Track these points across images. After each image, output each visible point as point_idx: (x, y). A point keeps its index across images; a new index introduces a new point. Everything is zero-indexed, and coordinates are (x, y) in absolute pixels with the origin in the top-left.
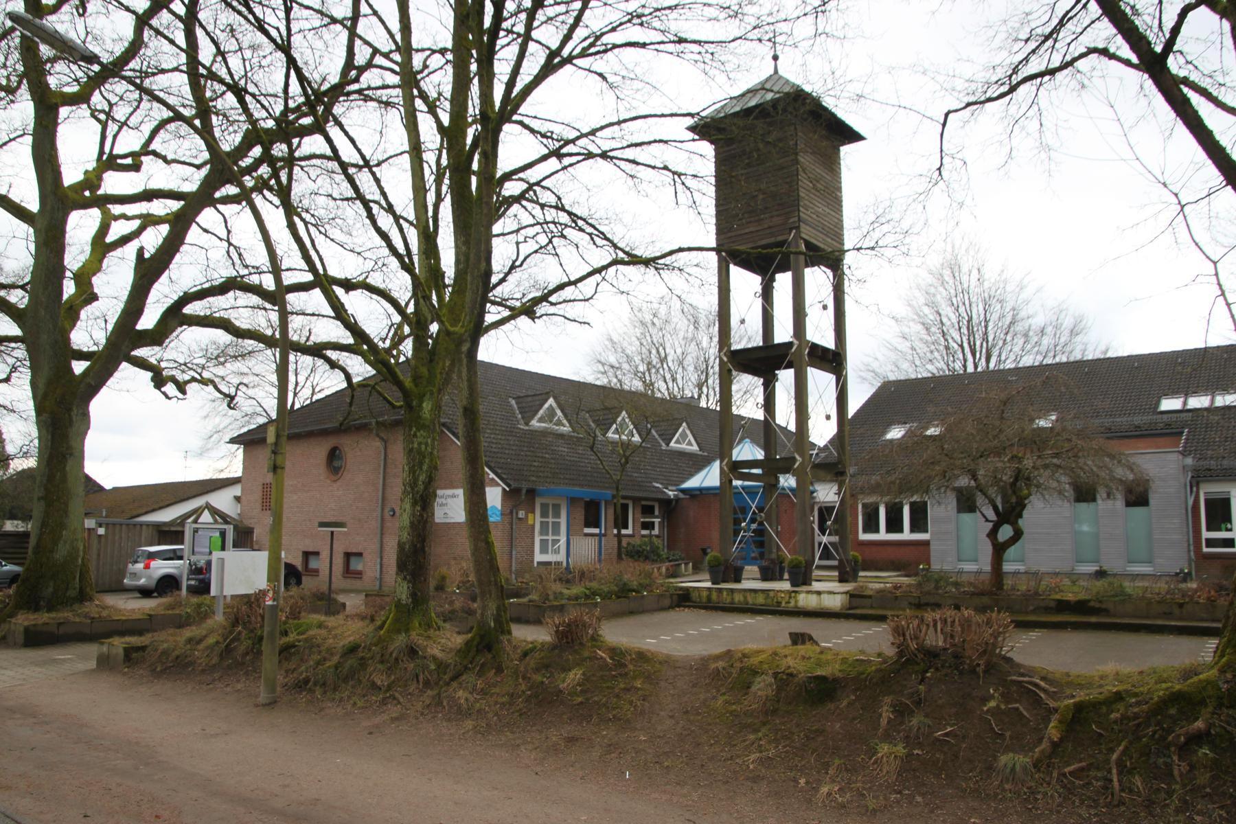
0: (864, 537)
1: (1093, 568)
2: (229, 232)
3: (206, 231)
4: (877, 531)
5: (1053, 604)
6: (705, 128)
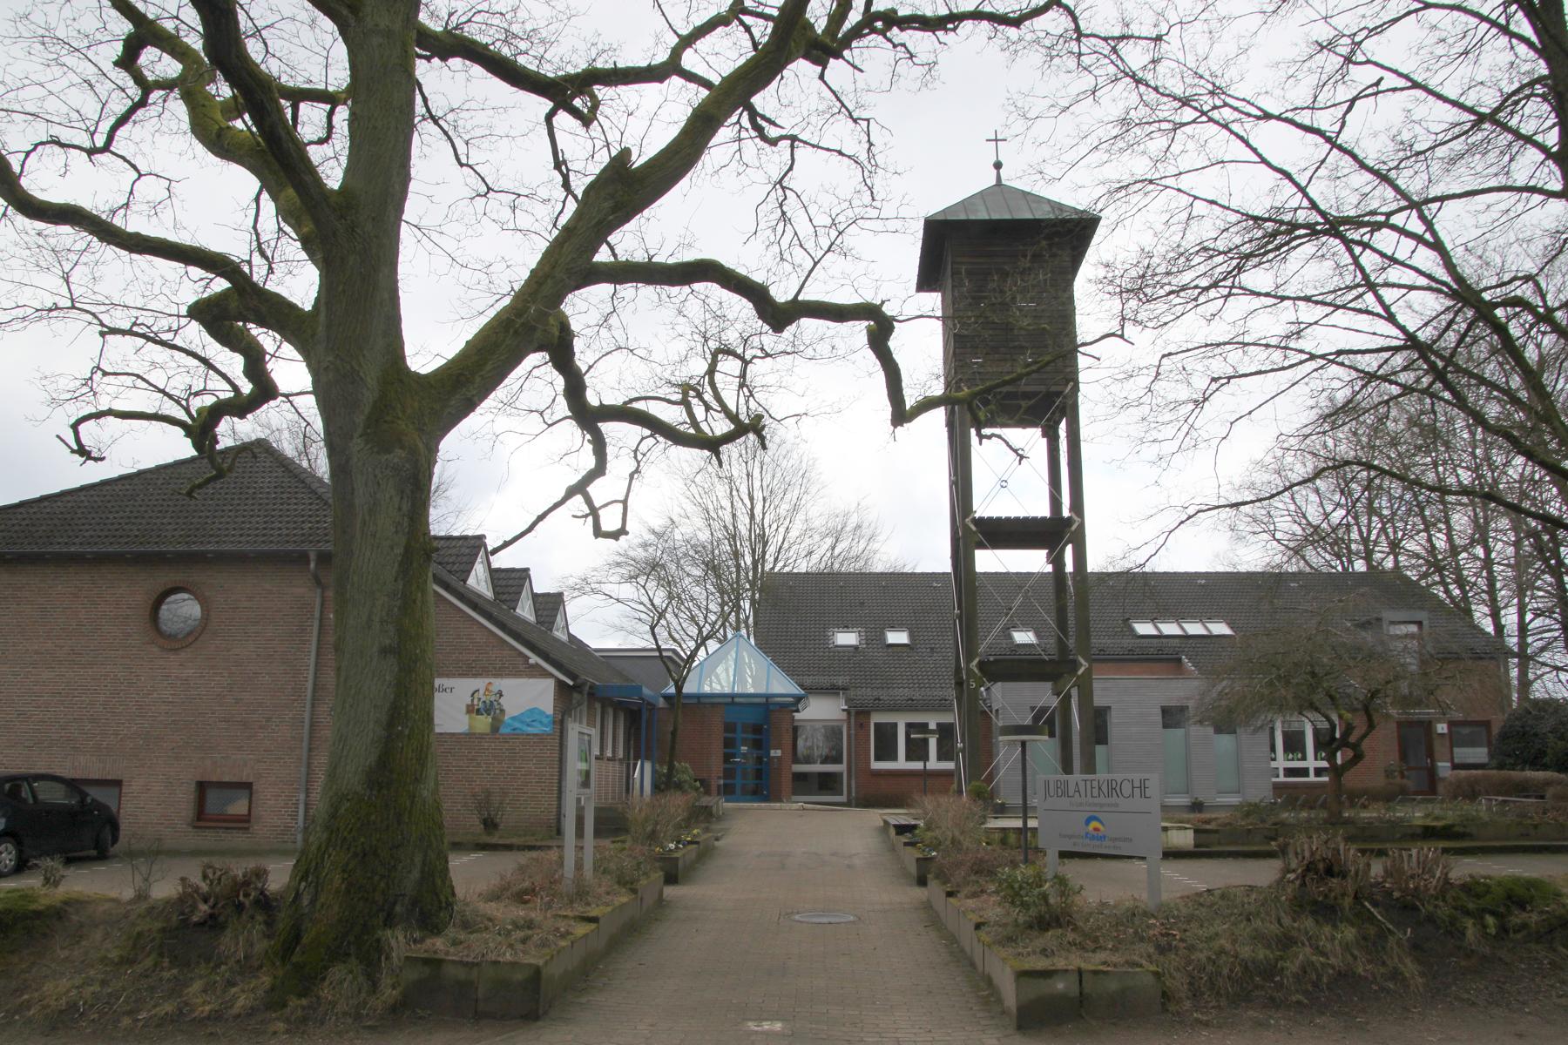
1: (1184, 800)
3: (1212, 202)
4: (894, 758)
5: (1419, 831)
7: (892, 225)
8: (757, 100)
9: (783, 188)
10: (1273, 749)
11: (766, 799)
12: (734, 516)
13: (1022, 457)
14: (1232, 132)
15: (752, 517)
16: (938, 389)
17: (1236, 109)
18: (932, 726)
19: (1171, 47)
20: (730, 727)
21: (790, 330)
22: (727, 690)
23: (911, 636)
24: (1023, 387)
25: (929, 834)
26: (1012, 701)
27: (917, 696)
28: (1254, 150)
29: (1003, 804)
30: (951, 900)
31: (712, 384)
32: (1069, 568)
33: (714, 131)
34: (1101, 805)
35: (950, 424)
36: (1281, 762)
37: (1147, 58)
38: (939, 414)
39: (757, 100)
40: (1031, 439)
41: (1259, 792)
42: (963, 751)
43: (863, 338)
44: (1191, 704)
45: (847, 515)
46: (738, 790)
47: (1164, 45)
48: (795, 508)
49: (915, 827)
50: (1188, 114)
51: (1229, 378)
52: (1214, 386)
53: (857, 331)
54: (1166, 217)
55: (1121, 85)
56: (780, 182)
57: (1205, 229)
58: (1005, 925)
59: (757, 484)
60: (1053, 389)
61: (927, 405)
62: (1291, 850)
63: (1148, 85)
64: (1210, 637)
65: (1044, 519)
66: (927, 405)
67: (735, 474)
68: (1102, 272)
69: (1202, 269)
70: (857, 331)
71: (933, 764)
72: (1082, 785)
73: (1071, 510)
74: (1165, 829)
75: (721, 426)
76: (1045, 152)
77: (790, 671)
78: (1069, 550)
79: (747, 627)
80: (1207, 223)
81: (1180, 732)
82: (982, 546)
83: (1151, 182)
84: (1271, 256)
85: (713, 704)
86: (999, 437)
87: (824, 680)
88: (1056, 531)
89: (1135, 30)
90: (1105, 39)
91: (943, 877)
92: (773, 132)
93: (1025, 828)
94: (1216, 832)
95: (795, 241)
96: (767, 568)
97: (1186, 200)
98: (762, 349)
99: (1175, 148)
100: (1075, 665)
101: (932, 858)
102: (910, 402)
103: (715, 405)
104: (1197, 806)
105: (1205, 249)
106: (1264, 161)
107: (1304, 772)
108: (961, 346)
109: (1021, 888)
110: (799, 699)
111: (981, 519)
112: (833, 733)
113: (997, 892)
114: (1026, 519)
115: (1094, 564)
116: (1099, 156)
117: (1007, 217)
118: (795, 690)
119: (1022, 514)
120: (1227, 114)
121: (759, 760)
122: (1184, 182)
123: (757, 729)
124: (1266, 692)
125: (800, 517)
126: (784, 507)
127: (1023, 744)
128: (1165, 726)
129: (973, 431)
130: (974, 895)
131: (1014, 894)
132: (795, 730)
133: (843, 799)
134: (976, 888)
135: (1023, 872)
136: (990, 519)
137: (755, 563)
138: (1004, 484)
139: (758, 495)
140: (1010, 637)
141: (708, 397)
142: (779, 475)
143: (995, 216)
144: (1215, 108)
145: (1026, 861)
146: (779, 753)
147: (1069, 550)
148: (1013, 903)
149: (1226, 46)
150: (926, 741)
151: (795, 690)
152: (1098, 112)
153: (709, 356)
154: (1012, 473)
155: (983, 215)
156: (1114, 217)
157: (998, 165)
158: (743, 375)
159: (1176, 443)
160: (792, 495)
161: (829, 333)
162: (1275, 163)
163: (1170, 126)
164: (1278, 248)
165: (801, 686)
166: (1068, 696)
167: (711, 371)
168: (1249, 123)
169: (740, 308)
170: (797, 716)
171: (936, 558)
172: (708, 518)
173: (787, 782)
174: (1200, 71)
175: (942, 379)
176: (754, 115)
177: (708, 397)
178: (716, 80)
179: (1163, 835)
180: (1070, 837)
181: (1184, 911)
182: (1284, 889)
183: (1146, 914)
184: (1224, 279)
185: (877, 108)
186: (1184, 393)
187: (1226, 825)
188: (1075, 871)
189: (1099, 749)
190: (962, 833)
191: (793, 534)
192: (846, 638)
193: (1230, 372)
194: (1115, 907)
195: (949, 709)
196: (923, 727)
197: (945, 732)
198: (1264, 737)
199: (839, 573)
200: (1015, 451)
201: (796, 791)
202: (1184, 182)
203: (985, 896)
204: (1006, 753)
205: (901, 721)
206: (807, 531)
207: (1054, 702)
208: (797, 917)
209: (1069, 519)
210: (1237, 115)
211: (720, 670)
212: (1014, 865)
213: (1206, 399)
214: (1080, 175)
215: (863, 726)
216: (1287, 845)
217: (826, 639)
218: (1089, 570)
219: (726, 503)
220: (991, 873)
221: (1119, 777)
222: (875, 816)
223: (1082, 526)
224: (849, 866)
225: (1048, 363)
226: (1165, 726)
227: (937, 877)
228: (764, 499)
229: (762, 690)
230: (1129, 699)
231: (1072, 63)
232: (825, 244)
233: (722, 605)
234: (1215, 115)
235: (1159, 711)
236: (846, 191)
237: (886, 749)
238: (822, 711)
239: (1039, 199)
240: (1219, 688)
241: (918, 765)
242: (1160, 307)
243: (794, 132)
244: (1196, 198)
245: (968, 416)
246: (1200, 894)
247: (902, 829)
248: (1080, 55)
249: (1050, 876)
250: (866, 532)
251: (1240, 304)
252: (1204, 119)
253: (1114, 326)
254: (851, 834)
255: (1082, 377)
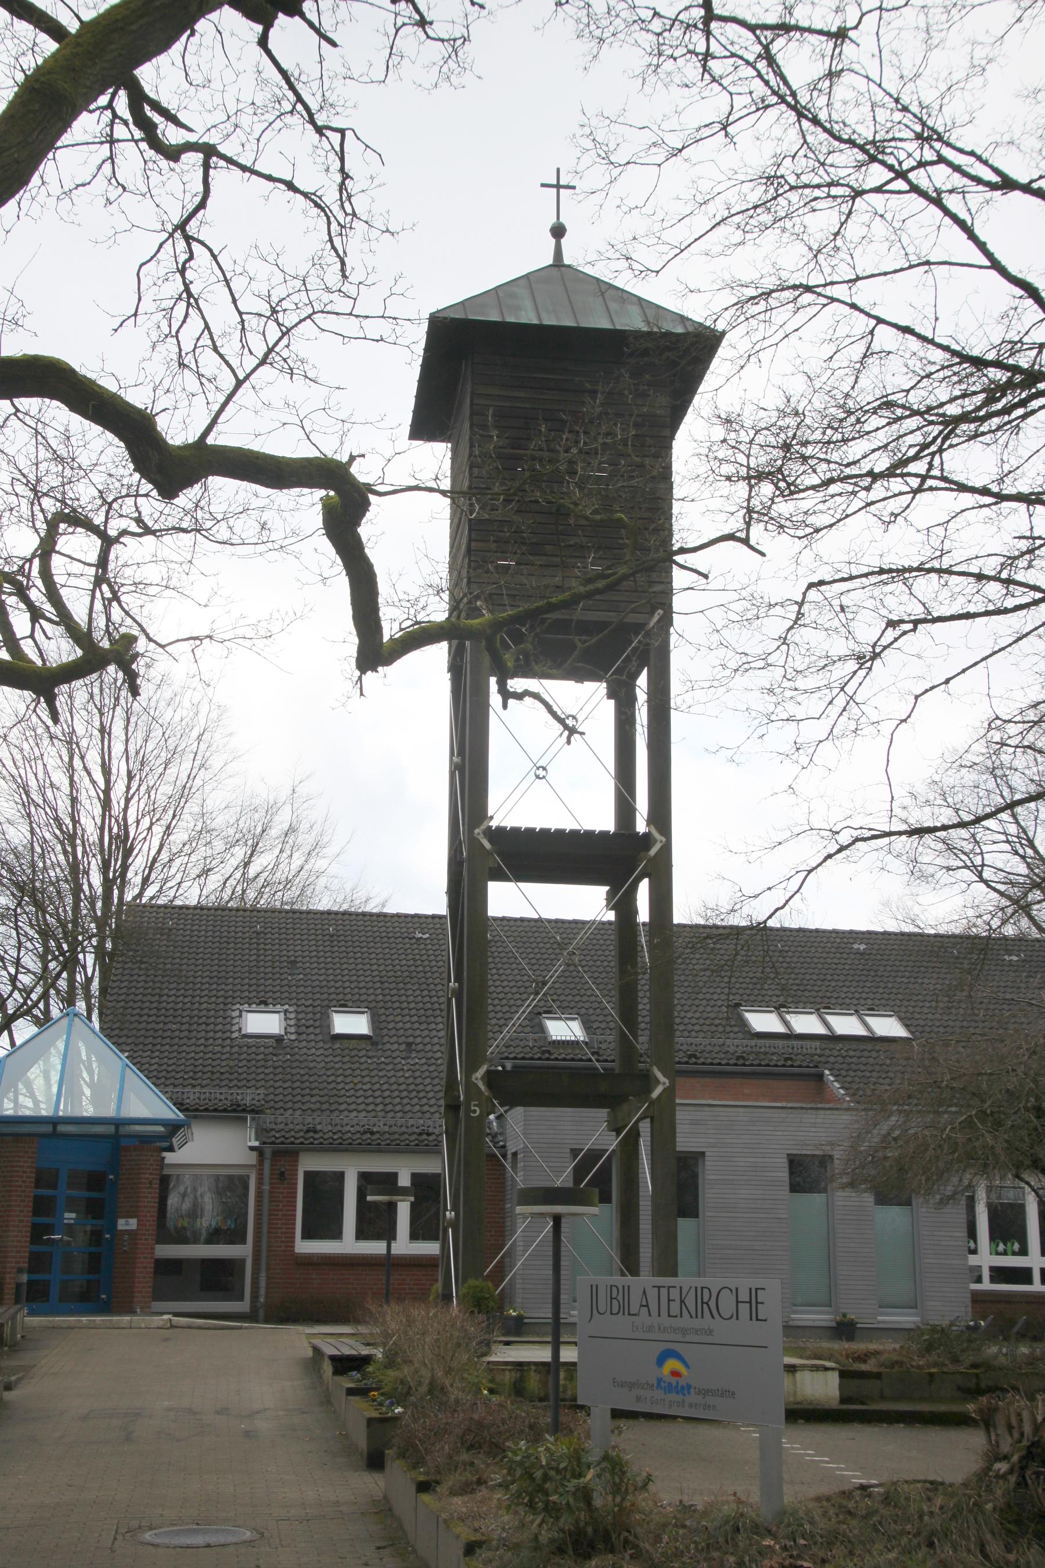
0: (305, 1247)
1: (822, 1318)
2: (104, 162)
3: (907, 330)
4: (336, 1234)
6: (723, 333)
7: (374, 329)
8: (146, 74)
9: (188, 239)
10: (972, 1234)
11: (106, 1308)
12: (74, 801)
13: (572, 731)
14: (947, 212)
15: (106, 804)
16: (438, 611)
17: (957, 169)
18: (404, 1181)
19: (857, 53)
20: (45, 1178)
21: (186, 498)
22: (45, 1111)
23: (374, 1022)
24: (579, 613)
25: (392, 1373)
26: (542, 1140)
27: (380, 1126)
28: (982, 246)
29: (520, 1319)
30: (426, 1498)
31: (46, 574)
32: (643, 915)
33: (65, 125)
34: (684, 1331)
35: (456, 669)
36: (986, 1258)
37: (820, 68)
38: (438, 653)
39: (146, 74)
40: (588, 700)
41: (948, 1308)
42: (454, 1224)
43: (315, 518)
44: (837, 1154)
45: (272, 810)
46: (55, 1291)
47: (848, 48)
48: (184, 794)
49: (367, 1360)
50: (877, 174)
51: (916, 623)
52: (891, 634)
53: (307, 505)
54: (829, 350)
55: (772, 113)
56: (182, 226)
57: (892, 376)
58: (517, 1547)
59: (118, 748)
60: (632, 618)
61: (419, 637)
62: (1000, 1420)
63: (815, 121)
64: (873, 1040)
65: (604, 834)
66: (419, 637)
67: (80, 728)
68: (719, 432)
69: (881, 438)
70: (307, 505)
71: (404, 1245)
72: (652, 1294)
73: (650, 822)
74: (791, 1369)
75: (60, 650)
76: (637, 224)
77: (159, 1078)
78: (644, 888)
79: (88, 997)
80: (894, 363)
81: (817, 1199)
82: (499, 876)
83: (808, 289)
84: (996, 421)
85: (18, 1137)
86: (536, 696)
87: (222, 1095)
88: (629, 855)
89: (801, 16)
90: (752, 28)
91: (413, 1454)
92: (173, 135)
93: (552, 1368)
94: (878, 1376)
95: (206, 340)
96: (128, 897)
97: (862, 323)
98: (139, 521)
99: (853, 230)
100: (647, 1081)
101: (396, 1419)
102: (391, 627)
103: (48, 608)
104: (845, 1329)
105: (889, 405)
106: (996, 265)
107: (1023, 1275)
108: (482, 539)
109: (546, 1478)
110: (174, 1127)
111: (501, 830)
112: (230, 1185)
113: (504, 1486)
114: (574, 833)
115: (685, 911)
116: (727, 233)
117: (568, 322)
118: (168, 1112)
119: (568, 825)
120: (940, 177)
121: (96, 1237)
122: (863, 293)
123: (95, 1181)
124: (960, 1137)
125: (192, 807)
126: (165, 789)
127: (557, 1219)
128: (794, 1188)
129: (493, 680)
130: (466, 1489)
131: (533, 1490)
132: (165, 1183)
133: (243, 1306)
134: (469, 1476)
135: (551, 1448)
136: (515, 831)
137: (108, 885)
138: (540, 772)
139: (119, 768)
140: (542, 1029)
141: (36, 595)
142: (157, 733)
143: (549, 320)
144: (922, 164)
145: (556, 1428)
146: (133, 1224)
147: (644, 888)
148: (531, 1505)
149: (950, 59)
150: (392, 1207)
151: (168, 1112)
152: (730, 158)
153: (42, 526)
154: (554, 755)
155: (528, 316)
156: (744, 346)
157: (558, 231)
158: (103, 562)
159: (825, 725)
160: (181, 769)
161: (256, 503)
162: (1013, 270)
163: (847, 191)
164: (1007, 410)
165: (180, 1105)
166: (634, 1135)
167: (47, 549)
168: (977, 196)
169: (102, 449)
170: (170, 1158)
171: (426, 894)
172: (27, 804)
173: (143, 1277)
174: (905, 100)
175: (446, 596)
176: (138, 98)
177: (36, 595)
178: (73, 26)
179: (787, 1379)
180: (632, 1385)
181: (823, 1524)
182: (989, 1490)
183: (760, 1529)
184: (916, 457)
185: (355, 107)
186: (840, 646)
187: (893, 1364)
188: (636, 1445)
189: (684, 1225)
190: (448, 1371)
191: (179, 837)
192: (262, 1023)
193: (918, 612)
194: (705, 1514)
195: (433, 1149)
196: (387, 1182)
197: (425, 1189)
198: (957, 1213)
199: (254, 910)
200: (561, 721)
201: (160, 1294)
202: (863, 293)
203: (483, 1492)
204: (527, 1230)
205: (350, 1173)
206: (203, 832)
207: (612, 1143)
208: (148, 1536)
209: (647, 836)
210: (958, 180)
211: (34, 1073)
212: (536, 1438)
213: (875, 656)
214: (695, 269)
215: (283, 1177)
216: (993, 1410)
217: (224, 1022)
218: (676, 920)
219: (60, 778)
220: (496, 1450)
221: (714, 1283)
222: (298, 1340)
223: (667, 850)
224: (247, 1434)
225: (625, 577)
226: (794, 1188)
227: (402, 1455)
228: (130, 777)
229: (109, 1111)
230: (736, 1139)
231: (692, 69)
232: (260, 350)
233: (43, 959)
234: (919, 177)
235: (784, 1163)
236: (297, 263)
237: (323, 1221)
238: (213, 1148)
239: (624, 296)
240: (884, 1128)
241: (376, 1248)
242: (809, 501)
243: (212, 138)
244: (880, 321)
245: (487, 659)
246: (846, 1494)
247: (344, 1364)
248: (707, 55)
249: (594, 1457)
250: (306, 840)
251: (938, 504)
252: (900, 185)
253: (735, 524)
254: (254, 1375)
255: (679, 602)
